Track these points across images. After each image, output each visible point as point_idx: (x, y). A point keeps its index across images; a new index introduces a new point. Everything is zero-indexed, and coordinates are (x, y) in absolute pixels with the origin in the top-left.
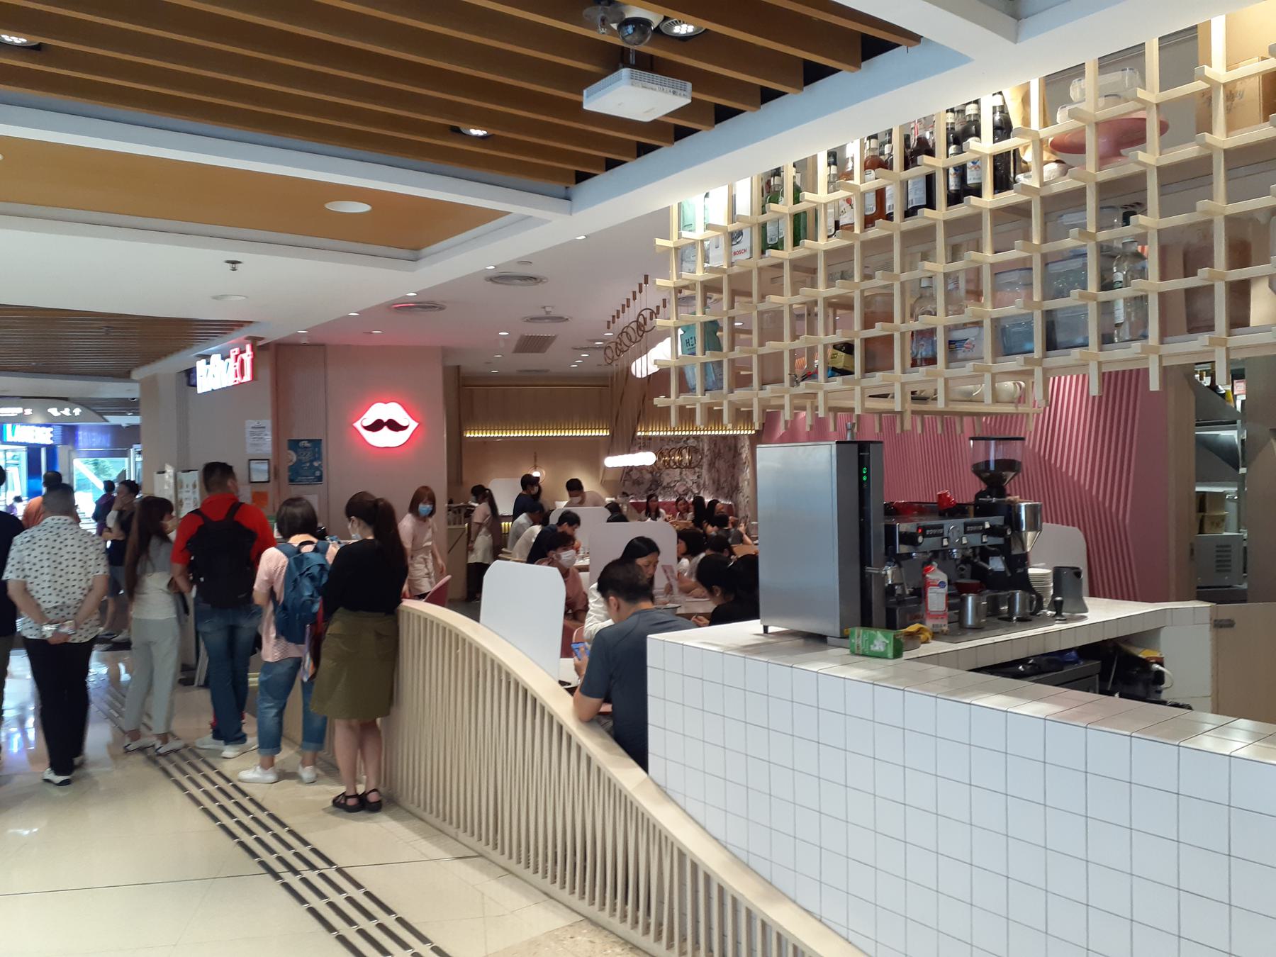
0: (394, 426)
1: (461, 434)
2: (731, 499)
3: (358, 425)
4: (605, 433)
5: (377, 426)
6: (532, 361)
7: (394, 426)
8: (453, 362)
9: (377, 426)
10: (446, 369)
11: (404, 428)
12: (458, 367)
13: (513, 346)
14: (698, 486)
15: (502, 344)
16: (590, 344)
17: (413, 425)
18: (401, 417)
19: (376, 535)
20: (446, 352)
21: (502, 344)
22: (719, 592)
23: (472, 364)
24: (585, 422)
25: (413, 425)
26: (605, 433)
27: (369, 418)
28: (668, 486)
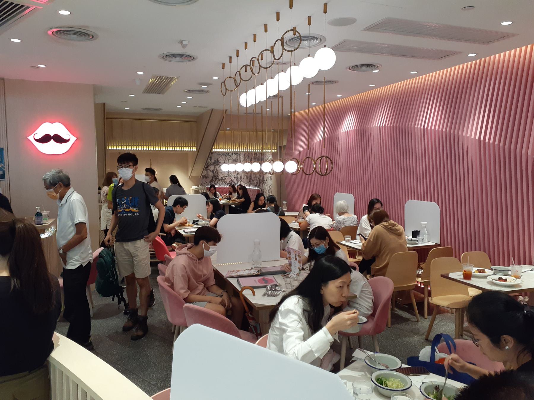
0: (59, 139)
1: (105, 148)
2: (259, 186)
3: (31, 138)
4: (194, 149)
5: (45, 139)
6: (154, 101)
7: (59, 139)
8: (101, 100)
9: (45, 139)
10: (96, 105)
11: (66, 141)
12: (104, 104)
13: (144, 87)
14: (237, 179)
15: (138, 82)
16: (198, 88)
17: (73, 139)
18: (64, 133)
19: (11, 271)
20: (96, 90)
21: (138, 82)
22: (509, 343)
23: (113, 103)
24: (182, 142)
25: (73, 139)
26: (194, 149)
27: (40, 133)
28: (222, 179)
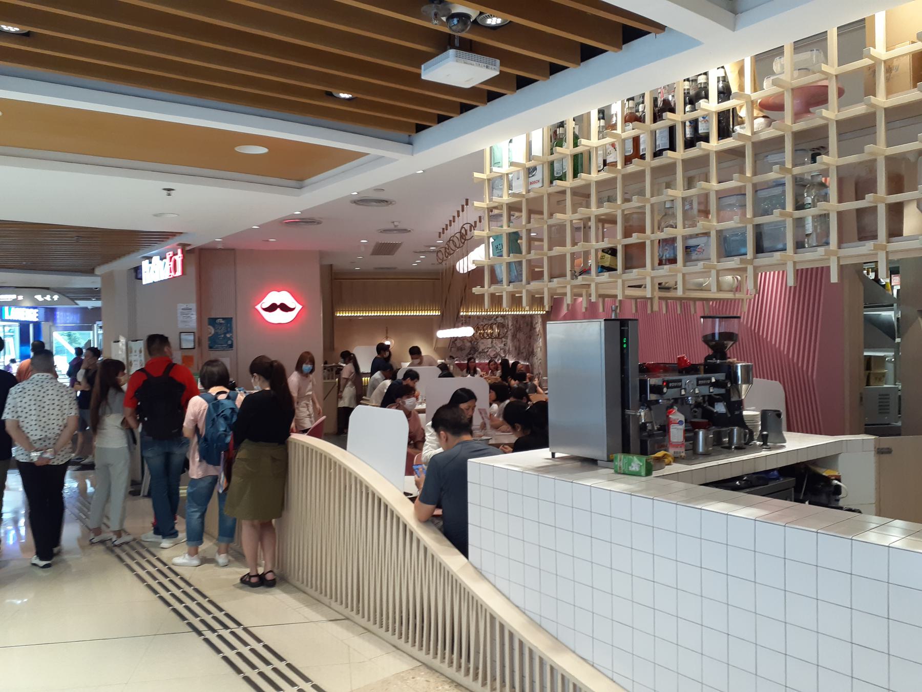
0: (285, 308)
1: (333, 314)
2: (528, 361)
3: (258, 307)
4: (438, 313)
5: (272, 308)
6: (384, 261)
7: (285, 308)
8: (327, 262)
9: (272, 308)
10: (322, 267)
11: (292, 309)
12: (331, 265)
13: (371, 250)
14: (505, 352)
15: (363, 249)
16: (426, 249)
17: (299, 307)
18: (290, 301)
19: (271, 387)
20: (322, 254)
21: (363, 249)
22: (519, 428)
23: (341, 264)
24: (423, 305)
25: (299, 307)
26: (438, 313)
27: (267, 302)
28: (483, 352)
